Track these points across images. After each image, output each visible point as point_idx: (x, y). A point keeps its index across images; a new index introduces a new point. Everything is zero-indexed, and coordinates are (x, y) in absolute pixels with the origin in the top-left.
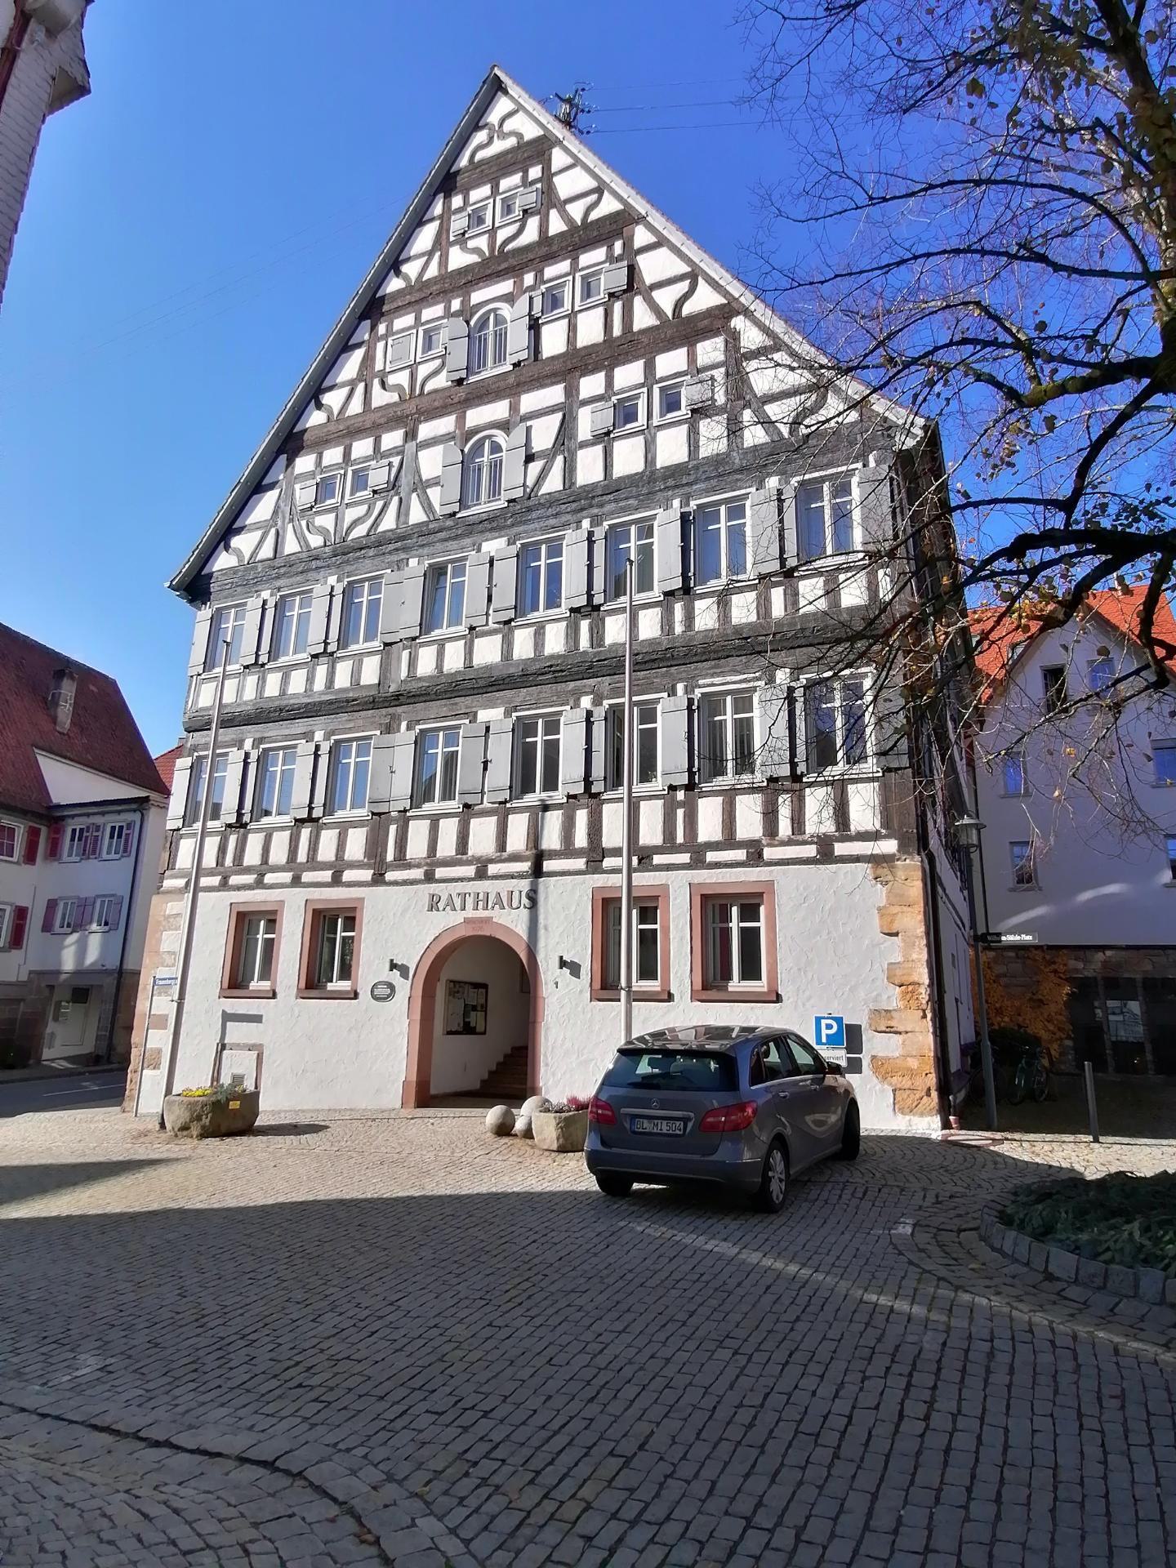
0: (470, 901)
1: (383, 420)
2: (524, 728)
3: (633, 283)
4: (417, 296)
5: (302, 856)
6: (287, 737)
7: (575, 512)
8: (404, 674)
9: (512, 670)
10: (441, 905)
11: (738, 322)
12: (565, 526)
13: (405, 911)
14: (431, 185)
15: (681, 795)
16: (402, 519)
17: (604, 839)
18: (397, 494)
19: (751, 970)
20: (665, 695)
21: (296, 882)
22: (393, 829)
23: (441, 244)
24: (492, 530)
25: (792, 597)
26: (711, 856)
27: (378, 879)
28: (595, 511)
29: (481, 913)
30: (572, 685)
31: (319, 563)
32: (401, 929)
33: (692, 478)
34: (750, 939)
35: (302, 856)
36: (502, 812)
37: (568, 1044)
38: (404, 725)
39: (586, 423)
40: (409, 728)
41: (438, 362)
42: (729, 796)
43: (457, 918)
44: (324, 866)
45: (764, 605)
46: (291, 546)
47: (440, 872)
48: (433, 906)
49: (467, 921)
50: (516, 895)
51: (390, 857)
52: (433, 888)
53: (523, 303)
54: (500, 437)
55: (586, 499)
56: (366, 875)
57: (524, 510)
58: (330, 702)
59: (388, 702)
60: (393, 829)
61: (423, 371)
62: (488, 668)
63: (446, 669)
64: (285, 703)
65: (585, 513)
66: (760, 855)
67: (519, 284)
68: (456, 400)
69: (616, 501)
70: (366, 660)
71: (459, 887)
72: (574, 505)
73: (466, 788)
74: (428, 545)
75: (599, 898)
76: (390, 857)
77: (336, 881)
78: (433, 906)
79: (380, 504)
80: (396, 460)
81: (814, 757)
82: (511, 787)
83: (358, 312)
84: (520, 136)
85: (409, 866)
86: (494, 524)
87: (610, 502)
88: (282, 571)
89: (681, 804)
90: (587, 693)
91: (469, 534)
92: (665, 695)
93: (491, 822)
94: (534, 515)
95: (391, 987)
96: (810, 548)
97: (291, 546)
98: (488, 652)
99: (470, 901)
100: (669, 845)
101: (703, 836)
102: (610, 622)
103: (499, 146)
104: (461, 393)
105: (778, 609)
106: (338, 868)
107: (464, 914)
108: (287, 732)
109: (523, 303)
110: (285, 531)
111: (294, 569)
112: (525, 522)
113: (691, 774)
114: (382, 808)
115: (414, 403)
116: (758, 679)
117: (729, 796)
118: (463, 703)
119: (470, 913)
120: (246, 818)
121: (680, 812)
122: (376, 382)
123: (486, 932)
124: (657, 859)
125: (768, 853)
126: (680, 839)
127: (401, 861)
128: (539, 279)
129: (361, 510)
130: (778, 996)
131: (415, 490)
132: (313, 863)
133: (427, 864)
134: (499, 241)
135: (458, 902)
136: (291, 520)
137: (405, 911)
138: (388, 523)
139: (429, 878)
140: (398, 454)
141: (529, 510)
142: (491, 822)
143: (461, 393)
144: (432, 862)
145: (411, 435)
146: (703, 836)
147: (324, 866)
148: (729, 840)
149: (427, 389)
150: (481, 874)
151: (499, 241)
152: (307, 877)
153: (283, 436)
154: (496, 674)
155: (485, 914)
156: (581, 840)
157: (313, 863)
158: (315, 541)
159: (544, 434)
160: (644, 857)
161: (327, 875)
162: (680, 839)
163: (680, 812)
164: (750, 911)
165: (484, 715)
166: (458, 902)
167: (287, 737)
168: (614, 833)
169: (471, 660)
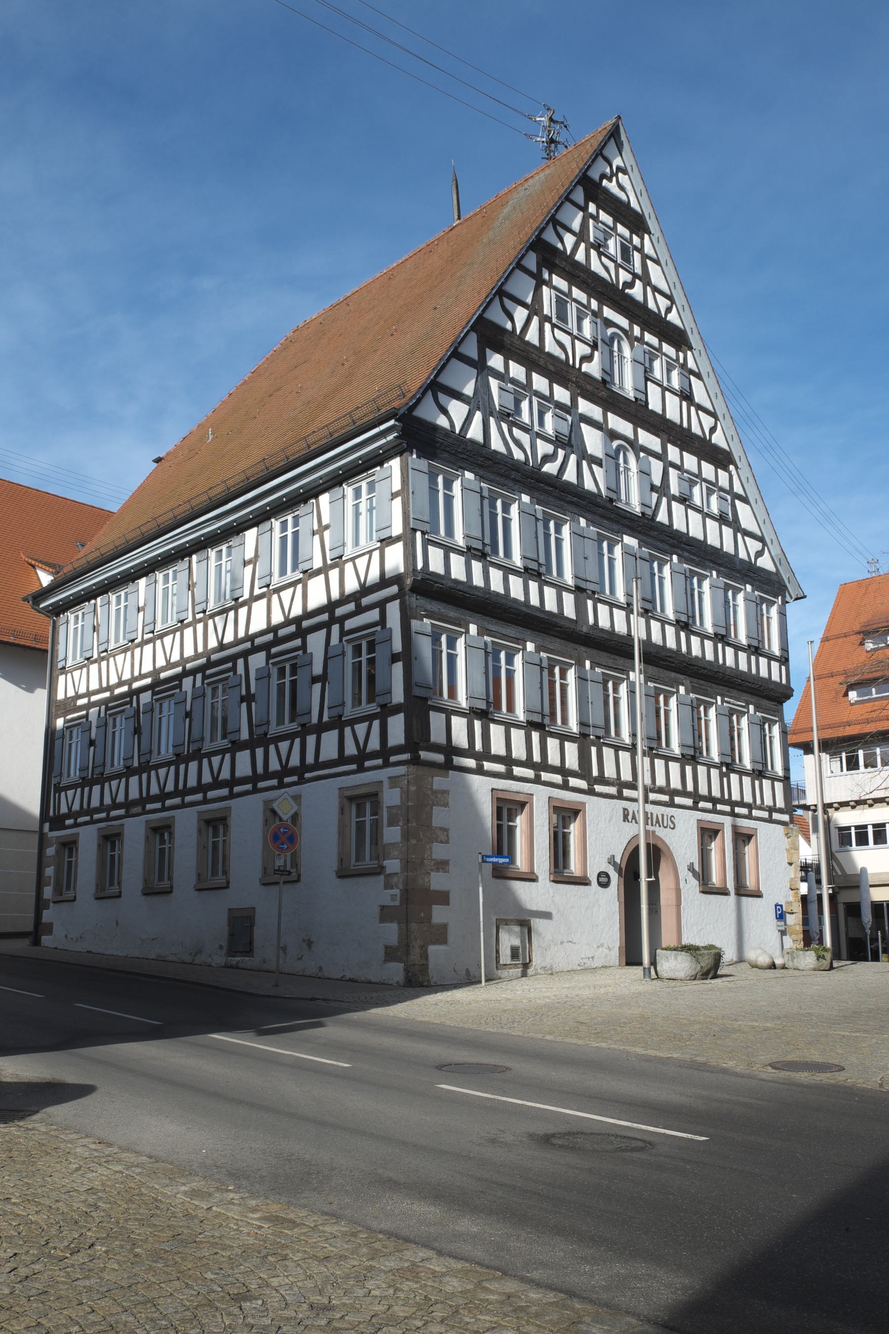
30: (673, 675)
65: (717, 567)
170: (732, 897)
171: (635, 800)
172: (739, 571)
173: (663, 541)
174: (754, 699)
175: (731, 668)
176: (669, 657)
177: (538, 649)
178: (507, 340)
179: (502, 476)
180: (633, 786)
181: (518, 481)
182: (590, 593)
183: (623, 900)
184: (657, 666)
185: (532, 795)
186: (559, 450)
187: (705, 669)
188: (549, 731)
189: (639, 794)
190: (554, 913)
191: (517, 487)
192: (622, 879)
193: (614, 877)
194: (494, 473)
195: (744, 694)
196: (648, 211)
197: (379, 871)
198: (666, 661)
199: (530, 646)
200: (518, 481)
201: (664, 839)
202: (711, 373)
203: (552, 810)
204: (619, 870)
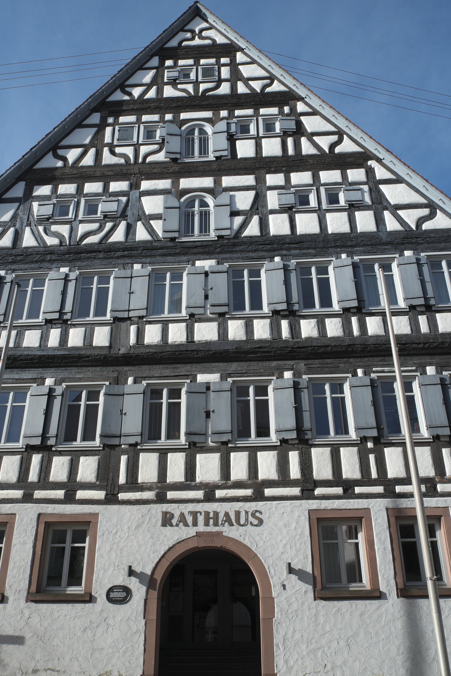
0: (201, 519)
1: (110, 173)
2: (240, 391)
3: (299, 131)
4: (139, 106)
5: (33, 476)
6: (18, 381)
7: (268, 251)
8: (132, 340)
9: (227, 347)
10: (174, 521)
11: (372, 163)
12: (264, 258)
13: (138, 526)
14: (151, 50)
15: (370, 445)
16: (130, 236)
17: (314, 474)
18: (14, 226)
19: (75, 578)
20: (350, 375)
21: (28, 498)
22: (124, 459)
23: (157, 81)
24: (203, 253)
25: (64, 338)
26: (268, 492)
27: (111, 499)
28: (285, 252)
29: (212, 529)
30: (274, 363)
31: (54, 257)
32: (131, 542)
33: (354, 243)
34: (77, 554)
35: (33, 476)
36: (134, 452)
37: (297, 636)
38: (130, 380)
39: (273, 200)
40: (135, 382)
41: (156, 147)
42: (253, 452)
43: (191, 532)
44: (57, 486)
45: (44, 338)
46: (28, 240)
47: (171, 495)
48: (167, 520)
49: (199, 535)
50: (243, 515)
51: (122, 479)
52: (165, 507)
53: (222, 126)
54: (209, 200)
55: (278, 244)
56: (100, 495)
57: (228, 246)
58: (63, 357)
59: (116, 361)
60: (124, 459)
61: (144, 150)
62: (208, 343)
63: (170, 340)
64: (18, 353)
65: (277, 252)
66: (435, 488)
67: (216, 114)
68: (171, 170)
69: (299, 249)
70: (97, 329)
71: (191, 507)
72: (268, 247)
73: (29, 434)
74: (151, 256)
75: (314, 517)
76: (122, 479)
77: (70, 498)
78: (167, 520)
79: (109, 225)
80: (124, 199)
81: (239, 431)
82: (142, 434)
83: (93, 105)
84: (214, 41)
85: (142, 488)
86: (206, 250)
87: (295, 249)
88: (19, 258)
89: (371, 451)
90: (288, 370)
91: (185, 254)
92: (350, 375)
93: (215, 458)
94: (238, 248)
95: (127, 591)
96: (82, 309)
97: (28, 240)
98: (206, 332)
99: (201, 519)
100: (365, 480)
101: (391, 474)
102: (72, 332)
103: (197, 42)
104: (176, 168)
105: (285, 333)
106: (71, 487)
107: (196, 529)
108: (17, 377)
109: (222, 126)
110: (23, 231)
111: (30, 258)
112: (231, 252)
113: (379, 428)
114: (115, 441)
115: (136, 167)
116: (415, 371)
117: (253, 452)
118: (183, 369)
119: (201, 528)
120: (52, 442)
121: (372, 457)
122: (106, 150)
123: (217, 544)
124: (358, 490)
125: (440, 488)
126: (374, 475)
127: (133, 484)
128: (231, 115)
129: (95, 226)
130: (91, 596)
131: (139, 220)
132: (44, 482)
133: (158, 488)
134: (201, 89)
135: (190, 519)
136: (29, 225)
137: (138, 526)
138: (118, 236)
139: (161, 499)
140: (124, 196)
141: (235, 245)
142: (215, 458)
143: (176, 168)
144: (162, 488)
145: (135, 186)
146: (391, 474)
147: (57, 486)
148: (337, 479)
149: (148, 160)
150: (209, 497)
151: (201, 89)
152: (38, 494)
153: (24, 168)
154: (214, 348)
155: (216, 529)
156: (295, 472)
157: (44, 482)
158: (51, 241)
159: (244, 201)
160: (348, 488)
161: (60, 494)
162: (374, 475)
163: (372, 457)
164: (80, 536)
165: (201, 378)
166: (190, 519)
167: (18, 381)
168: (322, 467)
169: (193, 337)
170: (393, 605)
171: (411, 495)
172: (387, 243)
173: (255, 251)
174: (427, 359)
175: (377, 336)
176: (260, 348)
177: (439, 371)
178: (57, 173)
179: (37, 262)
180: (407, 481)
181: (55, 260)
182: (136, 319)
183: (153, 615)
184: (246, 361)
185: (15, 514)
186: (39, 227)
187: (328, 346)
188: (56, 451)
189: (413, 488)
190: (28, 636)
191: (55, 265)
192: (154, 594)
193: (139, 591)
194: (27, 263)
195: (415, 358)
196: (233, 36)
197: (88, 598)
198: (256, 353)
199: (430, 370)
200: (55, 260)
201: (241, 539)
202: (323, 105)
203: (426, 519)
204: (150, 582)
